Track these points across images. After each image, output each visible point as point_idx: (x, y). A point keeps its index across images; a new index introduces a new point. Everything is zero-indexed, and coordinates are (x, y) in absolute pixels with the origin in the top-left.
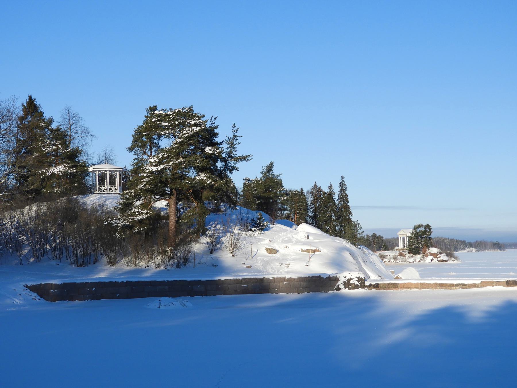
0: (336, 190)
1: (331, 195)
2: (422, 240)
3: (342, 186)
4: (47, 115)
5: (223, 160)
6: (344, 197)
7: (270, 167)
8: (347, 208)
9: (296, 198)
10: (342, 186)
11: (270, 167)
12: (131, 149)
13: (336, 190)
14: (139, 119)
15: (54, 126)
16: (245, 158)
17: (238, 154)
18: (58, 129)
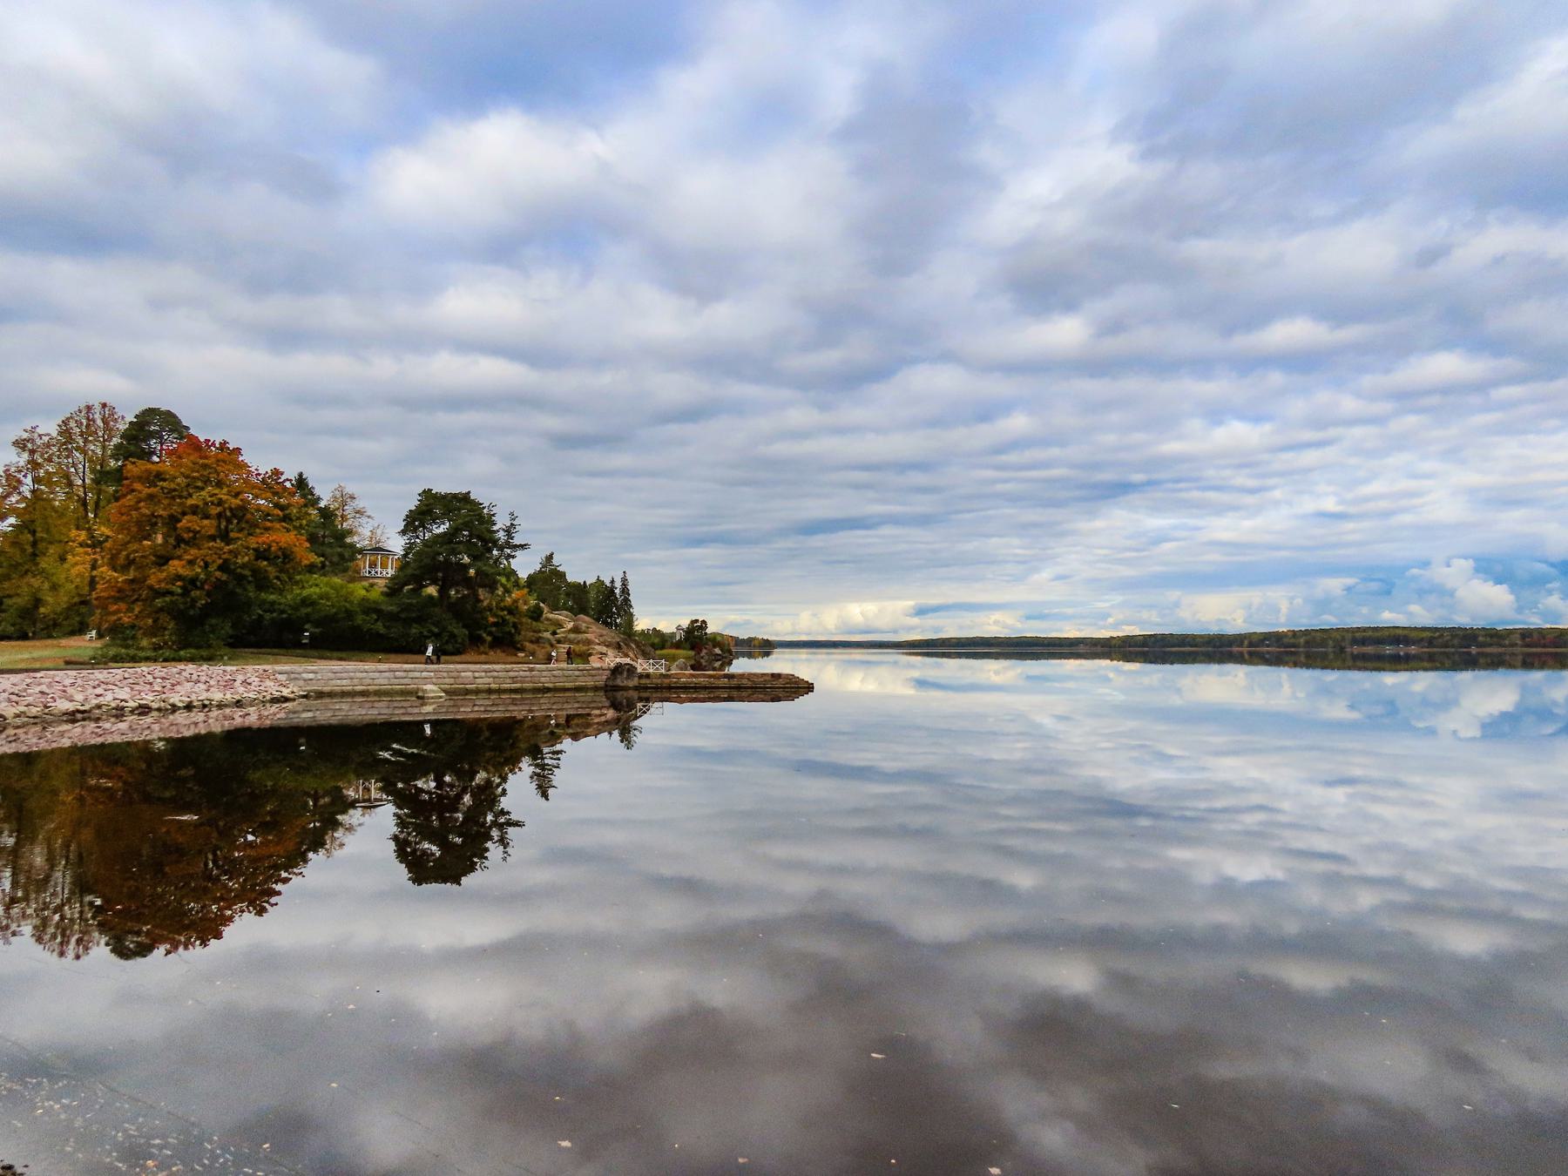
0: (618, 584)
1: (612, 590)
2: (189, 707)
3: (624, 581)
4: (317, 492)
5: (501, 549)
6: (625, 591)
7: (550, 558)
8: (627, 601)
9: (580, 590)
10: (624, 581)
11: (550, 558)
12: (403, 532)
13: (618, 584)
14: (413, 504)
15: (322, 505)
16: (522, 547)
17: (516, 541)
18: (327, 508)
